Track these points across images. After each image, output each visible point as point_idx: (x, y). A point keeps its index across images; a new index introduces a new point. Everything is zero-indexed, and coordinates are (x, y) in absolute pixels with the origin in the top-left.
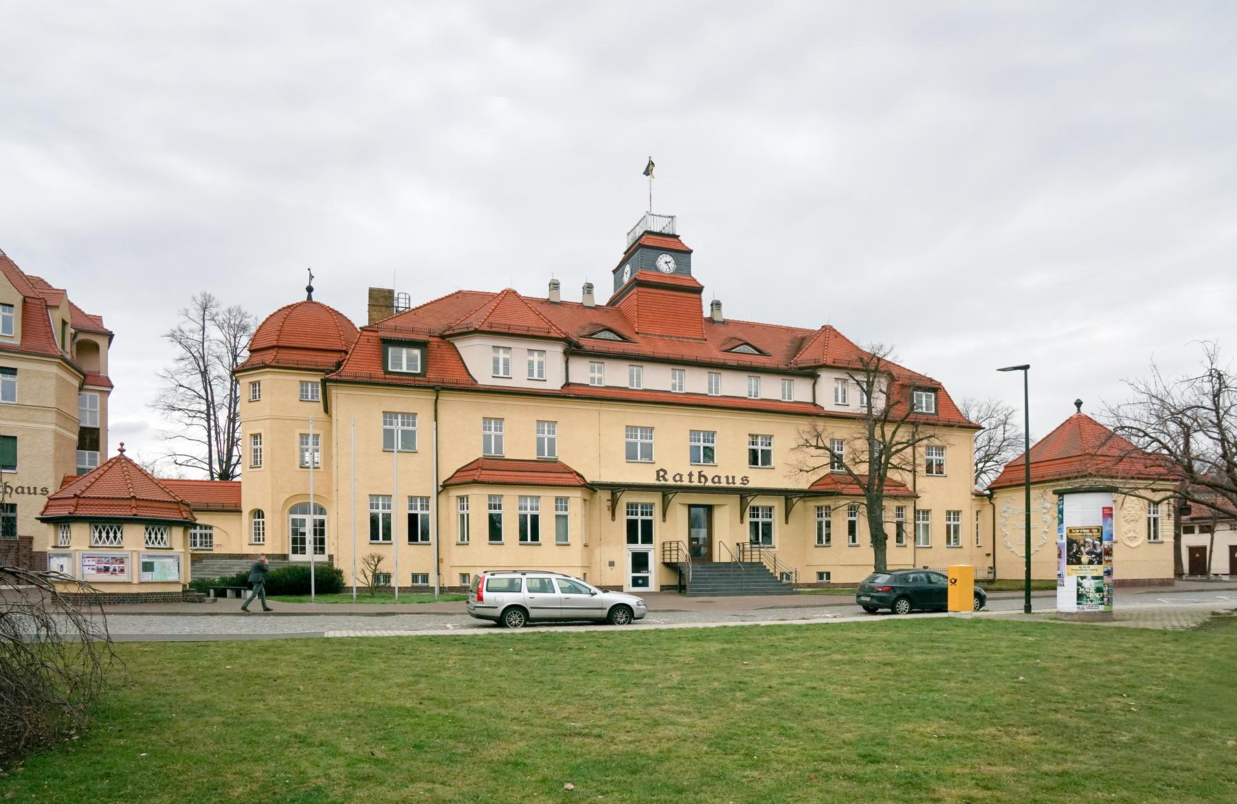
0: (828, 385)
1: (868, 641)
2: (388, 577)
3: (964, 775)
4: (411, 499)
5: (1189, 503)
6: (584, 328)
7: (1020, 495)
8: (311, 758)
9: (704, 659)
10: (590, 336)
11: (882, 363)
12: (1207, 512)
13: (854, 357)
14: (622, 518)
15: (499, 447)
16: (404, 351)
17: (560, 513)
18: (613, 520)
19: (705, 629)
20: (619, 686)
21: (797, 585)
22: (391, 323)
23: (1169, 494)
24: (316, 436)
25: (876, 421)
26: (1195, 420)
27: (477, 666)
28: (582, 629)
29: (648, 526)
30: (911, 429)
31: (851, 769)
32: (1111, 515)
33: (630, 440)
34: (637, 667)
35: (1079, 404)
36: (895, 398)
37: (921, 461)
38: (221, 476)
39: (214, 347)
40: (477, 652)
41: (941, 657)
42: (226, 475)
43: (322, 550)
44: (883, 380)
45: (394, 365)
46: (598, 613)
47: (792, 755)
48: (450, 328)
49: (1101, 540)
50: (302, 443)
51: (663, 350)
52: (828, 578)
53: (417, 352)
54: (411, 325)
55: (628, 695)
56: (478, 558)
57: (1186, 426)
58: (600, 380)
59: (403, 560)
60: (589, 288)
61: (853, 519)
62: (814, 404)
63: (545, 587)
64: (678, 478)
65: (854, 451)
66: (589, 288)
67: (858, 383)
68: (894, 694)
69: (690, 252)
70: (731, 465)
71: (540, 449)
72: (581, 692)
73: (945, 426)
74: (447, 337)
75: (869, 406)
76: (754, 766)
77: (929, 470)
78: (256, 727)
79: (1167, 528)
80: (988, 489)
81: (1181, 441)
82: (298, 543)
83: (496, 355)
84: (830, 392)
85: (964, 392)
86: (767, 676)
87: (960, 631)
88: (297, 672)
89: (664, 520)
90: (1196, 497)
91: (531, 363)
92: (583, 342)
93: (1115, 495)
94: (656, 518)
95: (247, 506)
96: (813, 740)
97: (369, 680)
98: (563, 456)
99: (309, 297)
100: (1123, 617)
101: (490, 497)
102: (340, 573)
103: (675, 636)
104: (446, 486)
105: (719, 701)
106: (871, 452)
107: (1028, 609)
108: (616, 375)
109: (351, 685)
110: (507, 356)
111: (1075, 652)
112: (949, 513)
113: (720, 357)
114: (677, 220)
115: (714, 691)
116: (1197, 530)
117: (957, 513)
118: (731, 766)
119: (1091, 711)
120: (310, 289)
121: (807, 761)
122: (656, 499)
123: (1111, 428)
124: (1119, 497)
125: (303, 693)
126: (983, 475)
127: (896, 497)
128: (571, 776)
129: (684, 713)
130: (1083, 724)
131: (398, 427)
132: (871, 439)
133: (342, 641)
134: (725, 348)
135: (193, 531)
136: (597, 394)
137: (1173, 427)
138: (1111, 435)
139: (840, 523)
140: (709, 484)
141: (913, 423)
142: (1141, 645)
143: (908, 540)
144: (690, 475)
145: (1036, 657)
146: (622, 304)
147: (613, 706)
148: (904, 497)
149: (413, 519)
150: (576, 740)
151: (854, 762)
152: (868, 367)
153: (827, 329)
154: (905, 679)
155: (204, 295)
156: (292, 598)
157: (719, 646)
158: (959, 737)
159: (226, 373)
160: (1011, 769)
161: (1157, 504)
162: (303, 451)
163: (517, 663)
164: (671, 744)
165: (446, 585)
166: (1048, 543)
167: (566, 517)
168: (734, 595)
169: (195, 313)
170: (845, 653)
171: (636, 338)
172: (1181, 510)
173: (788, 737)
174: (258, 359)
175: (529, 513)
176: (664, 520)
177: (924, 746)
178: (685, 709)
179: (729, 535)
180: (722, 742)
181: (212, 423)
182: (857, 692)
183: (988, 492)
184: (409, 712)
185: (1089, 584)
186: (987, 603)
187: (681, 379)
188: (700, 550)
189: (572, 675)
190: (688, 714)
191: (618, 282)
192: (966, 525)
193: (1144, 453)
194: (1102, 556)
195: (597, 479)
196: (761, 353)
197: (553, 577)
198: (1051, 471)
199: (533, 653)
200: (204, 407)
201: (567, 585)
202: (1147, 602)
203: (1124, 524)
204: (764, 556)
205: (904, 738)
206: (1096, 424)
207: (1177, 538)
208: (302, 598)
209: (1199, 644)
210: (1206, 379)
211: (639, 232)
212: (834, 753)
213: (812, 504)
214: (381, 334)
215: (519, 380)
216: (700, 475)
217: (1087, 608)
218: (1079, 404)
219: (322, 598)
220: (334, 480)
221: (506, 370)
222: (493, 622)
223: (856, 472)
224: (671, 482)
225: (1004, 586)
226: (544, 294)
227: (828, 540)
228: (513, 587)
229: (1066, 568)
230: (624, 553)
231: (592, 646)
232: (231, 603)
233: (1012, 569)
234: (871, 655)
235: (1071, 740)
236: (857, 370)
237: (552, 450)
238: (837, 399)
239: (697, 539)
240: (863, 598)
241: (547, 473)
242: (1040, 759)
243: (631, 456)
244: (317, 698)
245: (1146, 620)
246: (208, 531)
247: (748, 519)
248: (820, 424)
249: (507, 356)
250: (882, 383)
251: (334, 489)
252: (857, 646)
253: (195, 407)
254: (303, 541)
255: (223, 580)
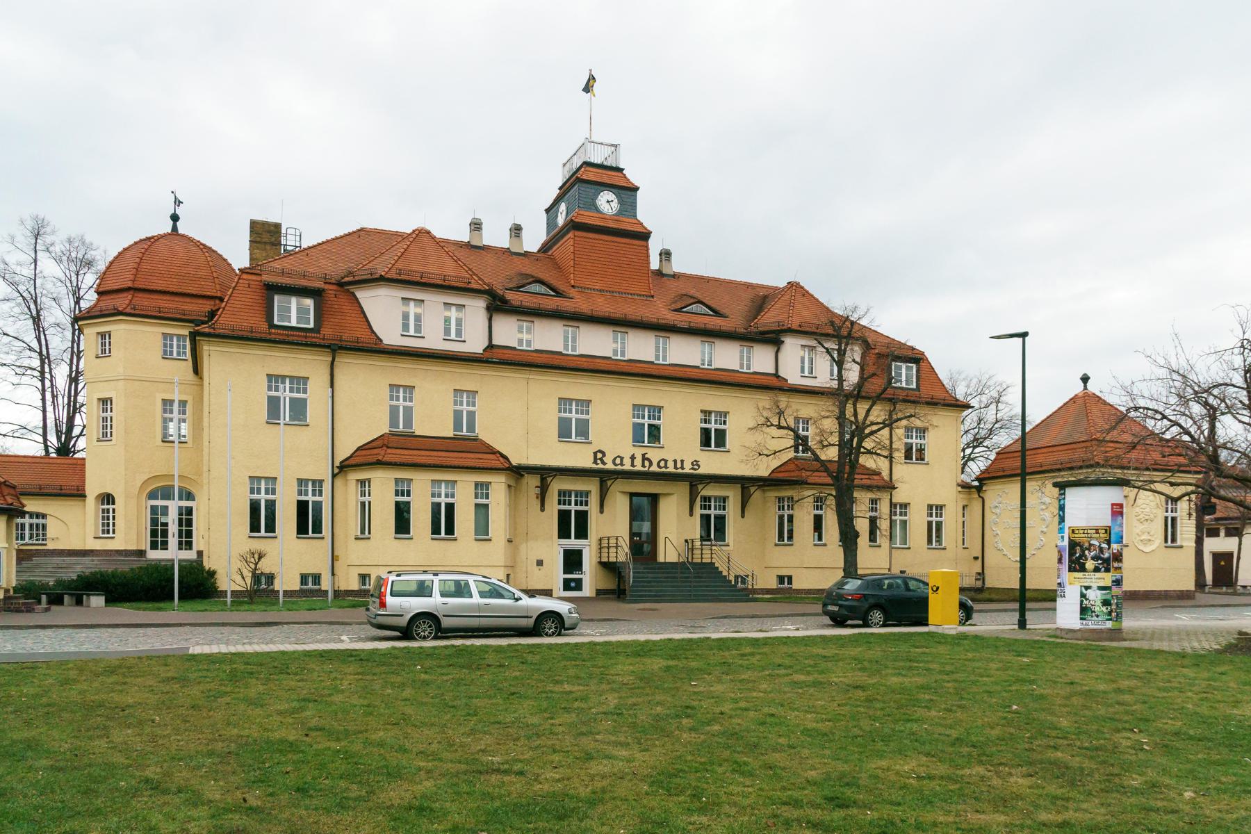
0: (793, 349)
1: (836, 659)
2: (270, 578)
3: (947, 825)
4: (301, 482)
5: (1213, 500)
6: (511, 279)
7: (1014, 488)
8: (166, 809)
9: (645, 679)
10: (518, 288)
11: (856, 328)
12: (1234, 511)
13: (823, 320)
14: (553, 508)
15: (408, 422)
16: (294, 301)
17: (480, 501)
18: (542, 510)
19: (647, 642)
20: (545, 711)
21: (754, 591)
22: (277, 265)
23: (1190, 488)
24: (183, 403)
25: (848, 396)
26: (1223, 400)
27: (377, 687)
28: (503, 642)
29: (582, 517)
30: (888, 407)
31: (816, 815)
32: (1121, 514)
33: (563, 415)
34: (567, 687)
35: (1085, 379)
36: (871, 369)
37: (899, 445)
38: (58, 451)
39: (49, 286)
40: (377, 670)
41: (920, 680)
42: (65, 450)
43: (189, 545)
44: (856, 348)
45: (281, 318)
46: (523, 623)
47: (746, 796)
48: (350, 273)
49: (1109, 542)
50: (165, 411)
51: (603, 306)
52: (790, 582)
53: (309, 302)
54: (301, 269)
55: (556, 721)
56: (378, 555)
57: (1212, 407)
58: (529, 342)
59: (290, 559)
60: (517, 230)
61: (819, 512)
62: (776, 375)
63: (461, 590)
64: (662, 464)
65: (822, 432)
66: (517, 230)
67: (828, 351)
68: (865, 724)
69: (636, 189)
70: (680, 447)
71: (457, 425)
72: (500, 718)
73: (928, 403)
74: (347, 285)
75: (840, 379)
76: (703, 810)
77: (908, 456)
78: (96, 771)
79: (1187, 530)
80: (977, 479)
81: (1206, 426)
82: (158, 536)
83: (405, 309)
84: (797, 361)
85: (948, 363)
86: (719, 699)
87: (942, 649)
88: (153, 699)
89: (602, 512)
90: (1222, 493)
91: (447, 320)
92: (510, 296)
93: (1127, 490)
94: (592, 508)
95: (93, 489)
96: (771, 778)
97: (242, 707)
98: (485, 433)
99: (175, 228)
100: (1135, 635)
101: (397, 481)
102: (212, 574)
103: (612, 651)
104: (343, 468)
105: (663, 730)
106: (841, 434)
107: (1022, 624)
108: (547, 337)
109: (219, 715)
110: (419, 310)
111: (1077, 677)
112: (930, 507)
113: (669, 317)
114: (622, 150)
115: (657, 718)
116: (1222, 533)
117: (940, 508)
118: (675, 810)
119: (1097, 749)
120: (175, 218)
121: (764, 804)
122: (592, 487)
123: (1123, 409)
124: (1131, 492)
125: (159, 725)
126: (971, 463)
127: (869, 488)
128: (486, 823)
129: (621, 744)
130: (1087, 764)
131: (285, 394)
132: (841, 418)
133: (211, 659)
134: (674, 306)
135: (19, 520)
136: (529, 359)
137: (1196, 409)
138: (1122, 418)
139: (804, 518)
140: (654, 468)
141: (890, 400)
142: (1154, 670)
143: (882, 540)
144: (633, 458)
145: (1032, 682)
146: (556, 251)
147: (538, 736)
148: (880, 488)
149: (302, 507)
150: (494, 778)
151: (818, 806)
152: (839, 332)
153: (793, 286)
154: (878, 705)
155: (36, 218)
156: (150, 605)
157: (664, 663)
158: (942, 778)
159: (66, 321)
160: (1002, 818)
161: (1175, 500)
162: (165, 421)
163: (426, 683)
164: (605, 783)
165: (342, 588)
166: (1046, 545)
167: (487, 506)
168: (681, 601)
169: (25, 240)
170: (809, 673)
171: (573, 292)
172: (1204, 508)
173: (743, 774)
174: (108, 303)
175: (443, 500)
176: (602, 512)
177: (901, 788)
178: (622, 739)
179: (676, 531)
180: (665, 781)
181: (48, 383)
182: (823, 721)
183: (976, 483)
184: (293, 747)
185: (1095, 596)
186: (975, 615)
187: (623, 343)
188: (644, 547)
189: (490, 697)
190: (625, 745)
191: (551, 223)
192: (950, 521)
193: (1161, 439)
194: (1110, 562)
195: (524, 462)
196: (717, 313)
197: (471, 579)
198: (1052, 459)
199: (444, 671)
200: (36, 363)
201: (487, 588)
202: (1161, 618)
203: (1138, 524)
204: (716, 555)
205: (877, 777)
206: (1105, 403)
207: (1199, 542)
208: (162, 605)
209: (1222, 669)
210: (1236, 351)
211: (577, 163)
212: (796, 794)
213: (773, 494)
214: (265, 278)
215: (433, 340)
216: (644, 458)
217: (1092, 624)
218: (1085, 379)
219: (188, 605)
220: (206, 458)
221: (418, 328)
222: (397, 634)
223: (823, 458)
224: (610, 466)
225: (994, 596)
226: (463, 235)
227: (790, 538)
228: (423, 590)
229: (1067, 576)
230: (553, 550)
231: (515, 662)
232: (67, 612)
233: (1003, 576)
234: (837, 677)
235: (1072, 784)
236: (827, 335)
237: (471, 427)
238: (802, 370)
239: (639, 535)
240: (830, 608)
241: (465, 453)
242: (1037, 806)
243: (564, 432)
244: (177, 730)
245: (1161, 640)
246: (41, 521)
247: (698, 512)
248: (783, 400)
249: (419, 310)
250: (855, 352)
251: (205, 469)
252: (823, 665)
253: (26, 363)
254: (165, 533)
255: (59, 583)
